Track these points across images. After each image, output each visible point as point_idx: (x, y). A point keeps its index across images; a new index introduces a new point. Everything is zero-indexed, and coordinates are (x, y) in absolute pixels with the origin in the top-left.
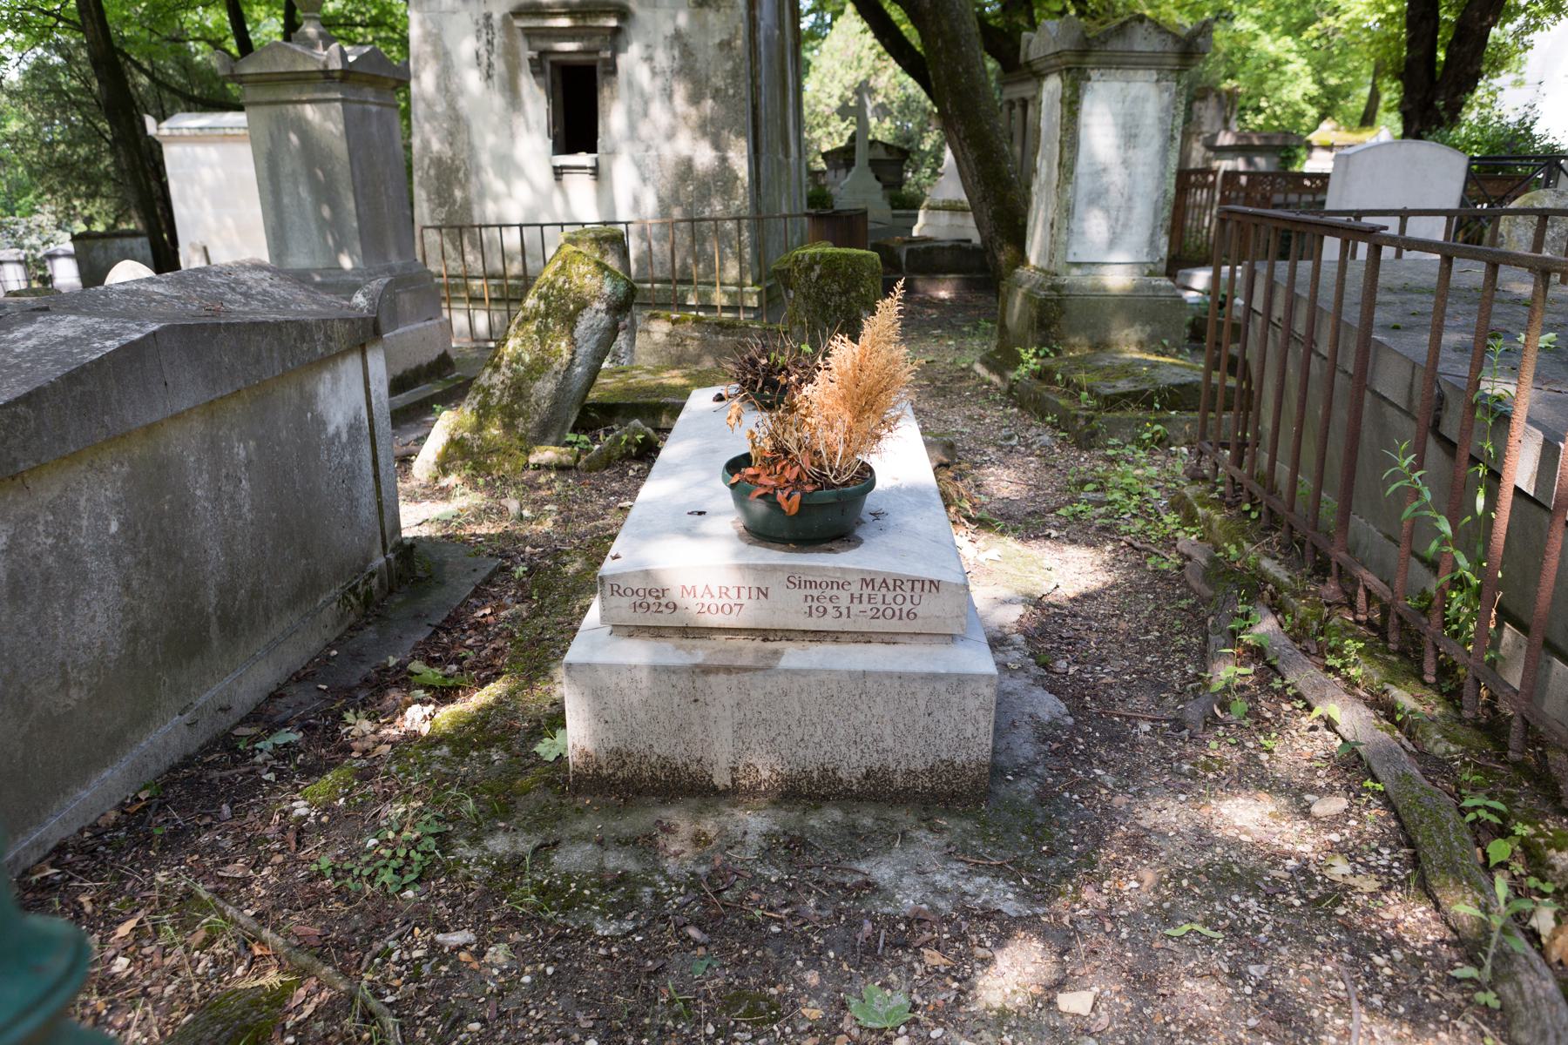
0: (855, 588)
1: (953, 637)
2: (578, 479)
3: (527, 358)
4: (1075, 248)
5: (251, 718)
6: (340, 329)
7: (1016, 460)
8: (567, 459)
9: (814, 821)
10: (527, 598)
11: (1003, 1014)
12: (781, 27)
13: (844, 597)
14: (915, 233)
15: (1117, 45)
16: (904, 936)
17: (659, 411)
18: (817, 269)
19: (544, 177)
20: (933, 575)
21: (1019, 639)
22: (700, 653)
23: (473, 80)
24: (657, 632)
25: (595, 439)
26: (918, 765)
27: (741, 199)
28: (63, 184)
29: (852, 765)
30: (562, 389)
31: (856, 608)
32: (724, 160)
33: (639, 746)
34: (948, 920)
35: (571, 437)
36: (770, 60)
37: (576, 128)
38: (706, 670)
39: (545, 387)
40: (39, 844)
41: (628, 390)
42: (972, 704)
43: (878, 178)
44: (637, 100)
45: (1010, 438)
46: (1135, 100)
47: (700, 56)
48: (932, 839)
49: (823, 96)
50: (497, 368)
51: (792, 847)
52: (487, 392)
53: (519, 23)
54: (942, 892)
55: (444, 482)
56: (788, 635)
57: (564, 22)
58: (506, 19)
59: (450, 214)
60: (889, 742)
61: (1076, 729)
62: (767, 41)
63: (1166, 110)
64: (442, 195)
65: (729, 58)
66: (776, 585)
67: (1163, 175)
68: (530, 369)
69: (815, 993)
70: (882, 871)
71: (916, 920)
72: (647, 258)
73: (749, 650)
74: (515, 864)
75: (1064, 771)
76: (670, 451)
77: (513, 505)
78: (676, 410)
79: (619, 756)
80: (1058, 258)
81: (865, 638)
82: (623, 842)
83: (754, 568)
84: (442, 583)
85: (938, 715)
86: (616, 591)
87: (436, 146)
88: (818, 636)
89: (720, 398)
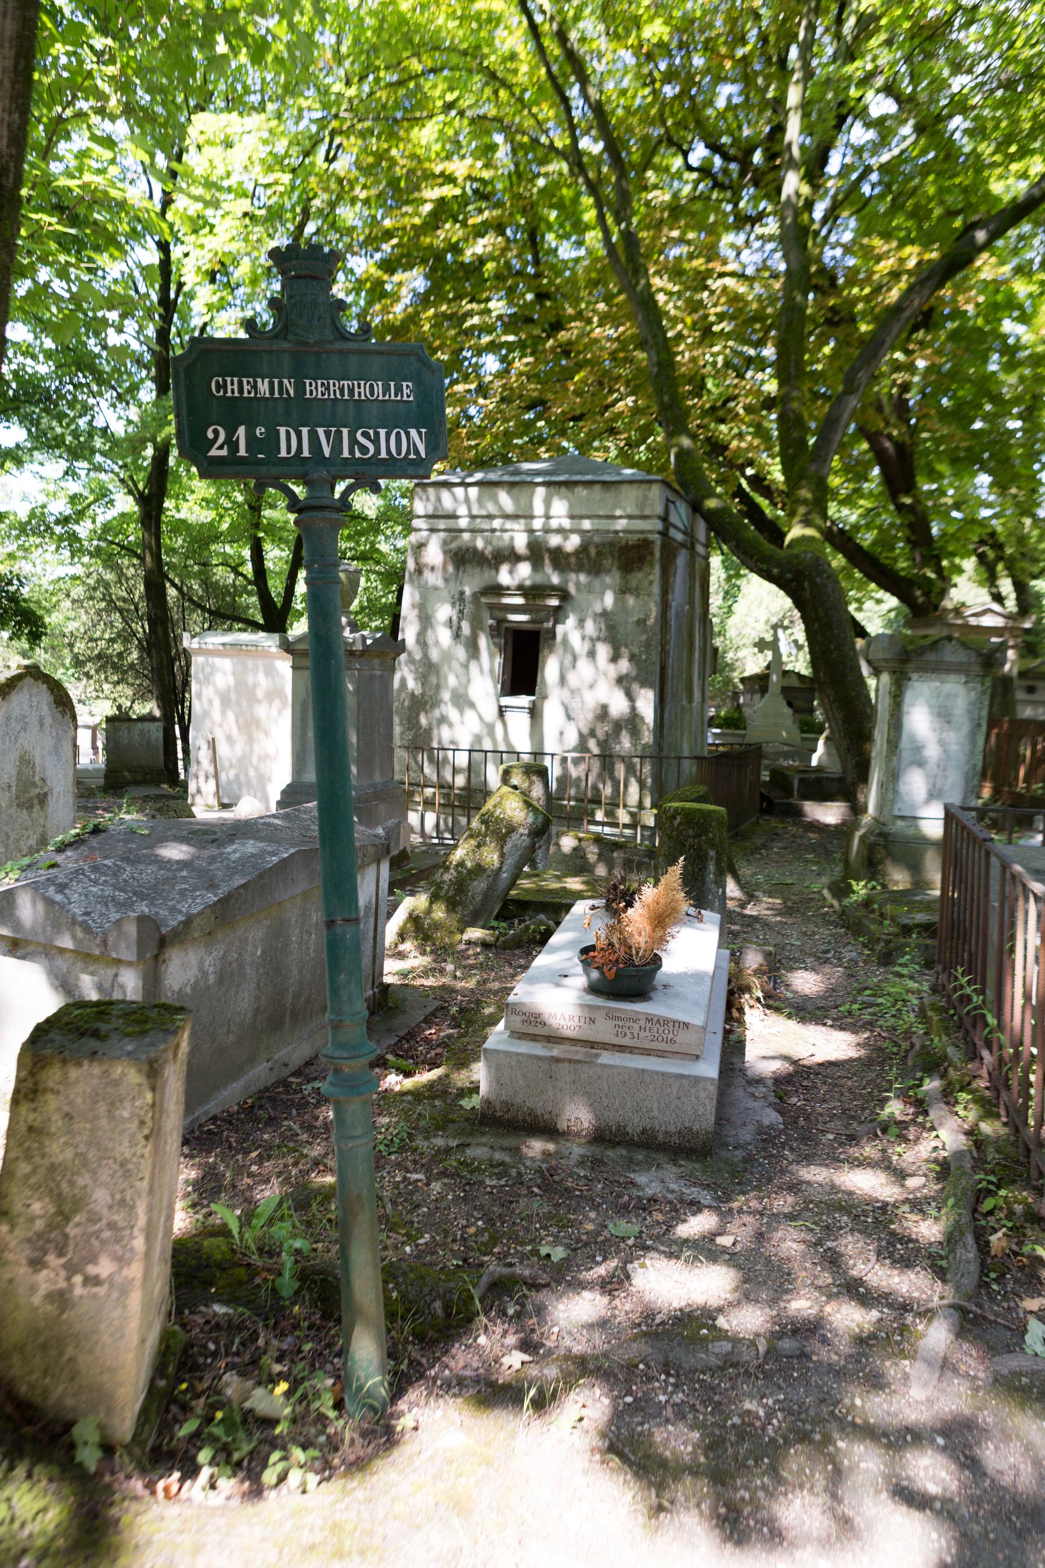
0: (642, 1023)
1: (697, 1057)
2: (496, 955)
3: (469, 864)
4: (899, 805)
5: (297, 1073)
6: (371, 850)
7: (827, 969)
8: (490, 939)
9: (610, 1153)
10: (457, 1026)
11: (686, 1241)
12: (691, 603)
13: (636, 1027)
14: (814, 762)
15: (931, 657)
16: (648, 1205)
17: (557, 908)
18: (679, 819)
19: (490, 712)
20: (686, 1019)
21: (770, 1083)
22: (556, 1051)
23: (444, 636)
24: (533, 1038)
25: (511, 926)
26: (672, 1129)
27: (647, 737)
28: (97, 671)
29: (635, 1125)
30: (490, 888)
31: (642, 1034)
32: (633, 708)
33: (518, 1100)
34: (670, 1202)
35: (495, 924)
36: (679, 629)
37: (522, 675)
38: (557, 1060)
39: (479, 886)
40: (206, 1113)
41: (540, 891)
42: (703, 1095)
43: (790, 704)
44: (569, 657)
45: (827, 952)
46: (948, 696)
47: (621, 630)
48: (674, 1169)
49: (750, 620)
50: (447, 869)
51: (596, 1163)
52: (439, 886)
53: (483, 600)
54: (673, 1192)
55: (401, 947)
56: (605, 1046)
57: (519, 601)
58: (476, 596)
59: (416, 736)
60: (656, 1113)
61: (784, 1131)
62: (677, 616)
63: (973, 704)
64: (412, 722)
65: (644, 632)
66: (599, 1016)
67: (972, 753)
68: (470, 872)
69: (593, 1221)
70: (641, 1179)
71: (653, 1200)
72: (564, 780)
73: (579, 1053)
74: (448, 1150)
75: (764, 1149)
76: (555, 939)
77: (450, 967)
78: (568, 908)
79: (507, 1105)
80: (885, 812)
81: (647, 1052)
82: (503, 1149)
83: (589, 1006)
84: (404, 1012)
85: (684, 1099)
86: (514, 1012)
87: (411, 684)
88: (621, 1048)
89: (593, 908)
